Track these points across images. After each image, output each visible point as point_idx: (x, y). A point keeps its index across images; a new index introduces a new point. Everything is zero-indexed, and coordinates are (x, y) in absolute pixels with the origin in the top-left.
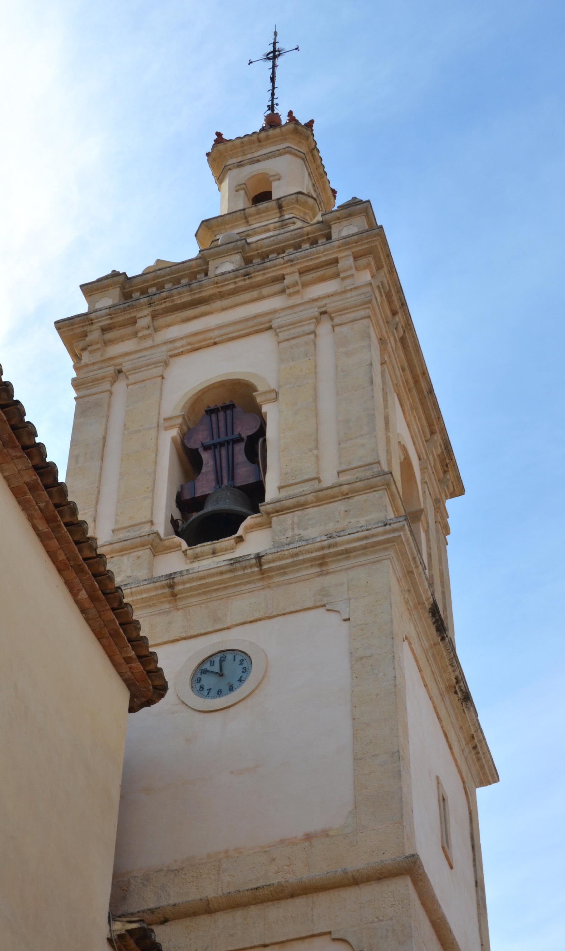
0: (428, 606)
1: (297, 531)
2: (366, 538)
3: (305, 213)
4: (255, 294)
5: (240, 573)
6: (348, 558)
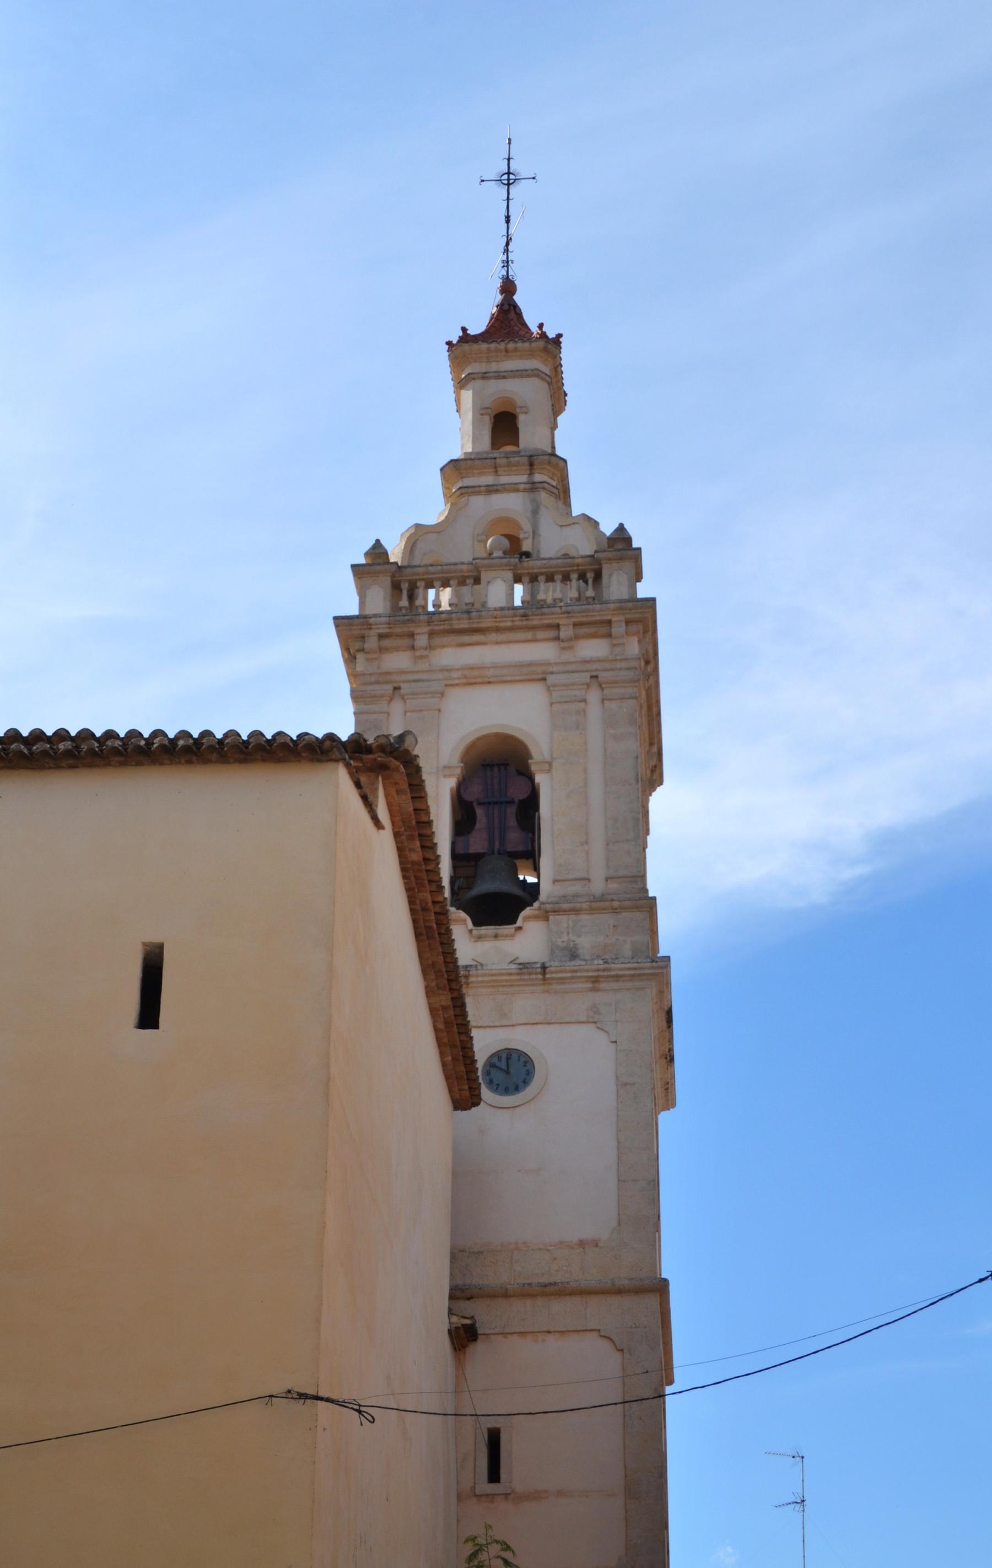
0: (666, 1008)
1: (572, 937)
2: (635, 969)
3: (554, 474)
4: (529, 635)
5: (526, 977)
6: (617, 981)
